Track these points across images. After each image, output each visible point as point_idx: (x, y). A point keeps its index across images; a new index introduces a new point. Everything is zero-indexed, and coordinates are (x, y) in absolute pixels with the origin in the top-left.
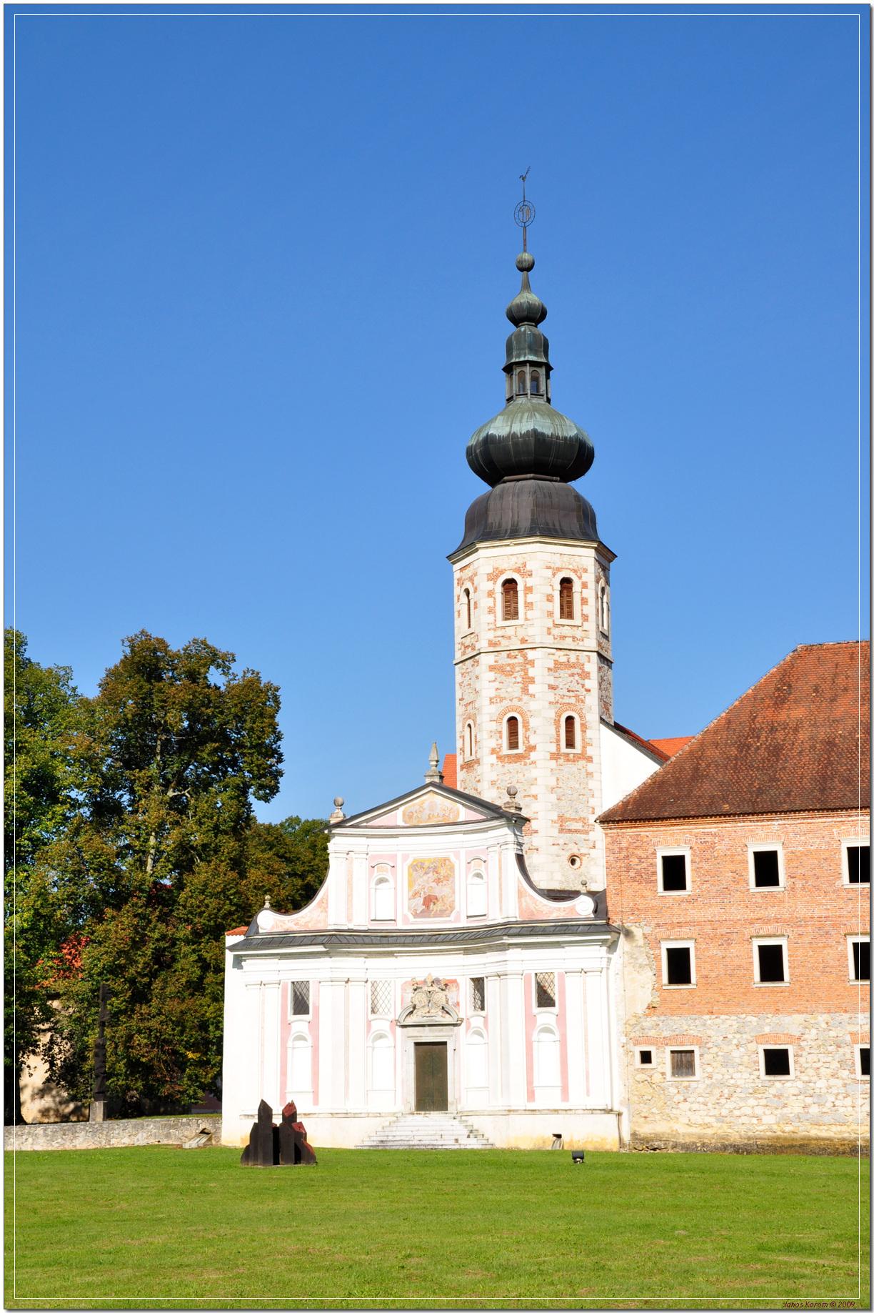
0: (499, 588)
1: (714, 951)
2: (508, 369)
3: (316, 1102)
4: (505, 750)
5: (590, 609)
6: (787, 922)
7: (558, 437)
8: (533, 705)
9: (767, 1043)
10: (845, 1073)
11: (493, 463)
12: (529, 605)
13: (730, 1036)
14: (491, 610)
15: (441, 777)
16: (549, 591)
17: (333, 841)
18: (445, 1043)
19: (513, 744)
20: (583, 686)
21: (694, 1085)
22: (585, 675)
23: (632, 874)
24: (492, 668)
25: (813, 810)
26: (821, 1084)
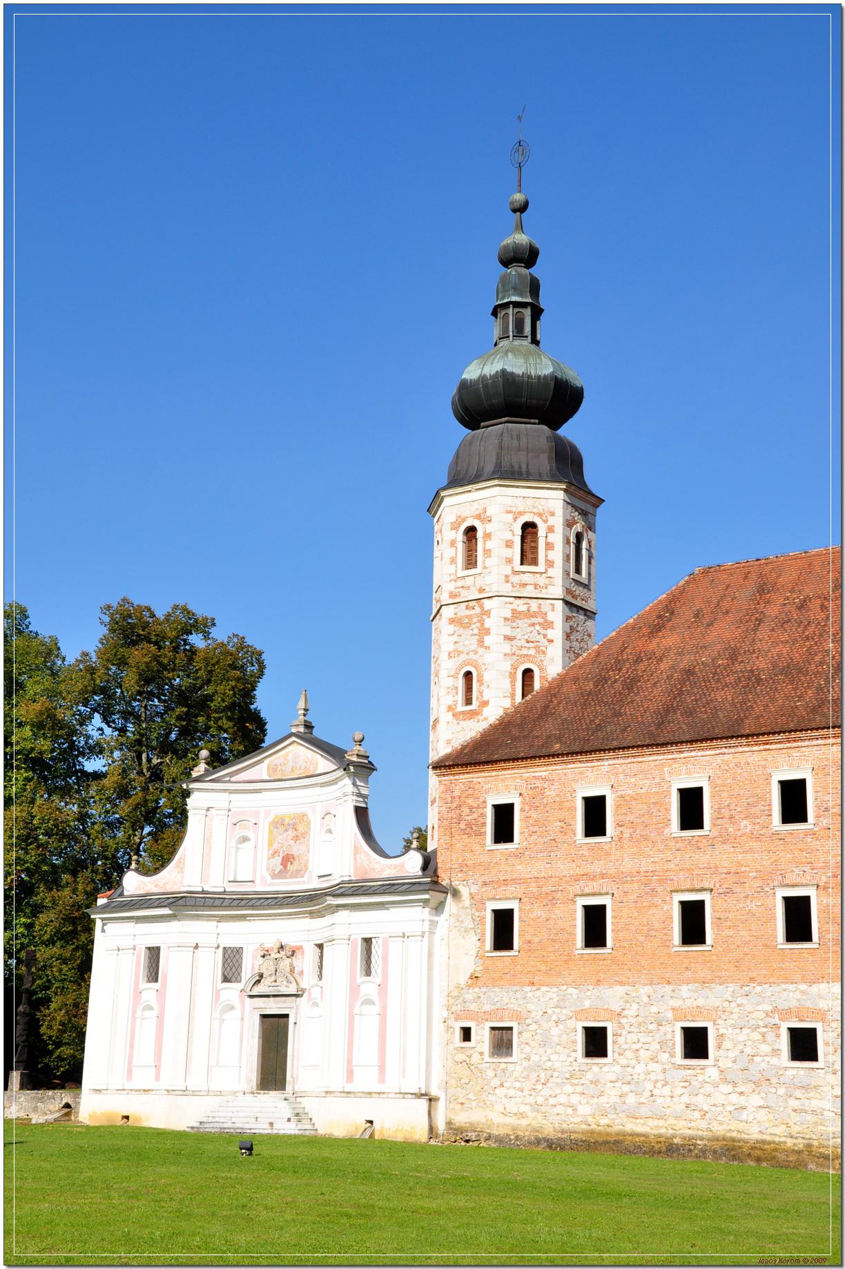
0: (460, 536)
1: (539, 912)
2: (495, 313)
3: (157, 1078)
4: (461, 707)
5: (557, 555)
6: (613, 878)
7: (529, 377)
9: (586, 1019)
10: (664, 1057)
11: (477, 408)
12: (487, 552)
13: (550, 1011)
16: (509, 536)
17: (192, 796)
19: (468, 701)
20: (545, 636)
21: (511, 1067)
22: (548, 625)
23: (463, 826)
24: (452, 621)
25: (643, 746)
26: (640, 1068)
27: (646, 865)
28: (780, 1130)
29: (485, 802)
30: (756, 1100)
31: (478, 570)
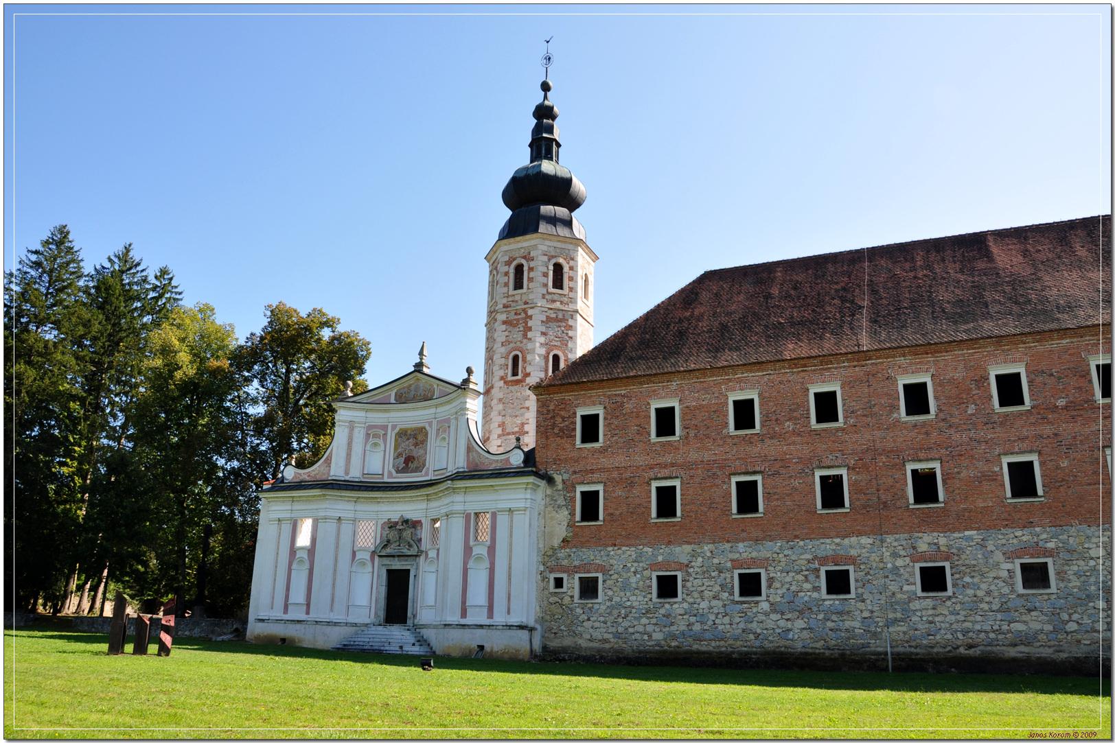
3: (308, 613)
4: (510, 378)
9: (660, 570)
14: (506, 285)
19: (515, 373)
21: (596, 606)
23: (556, 431)
24: (504, 323)
26: (704, 605)
27: (707, 456)
30: (800, 624)
31: (524, 290)
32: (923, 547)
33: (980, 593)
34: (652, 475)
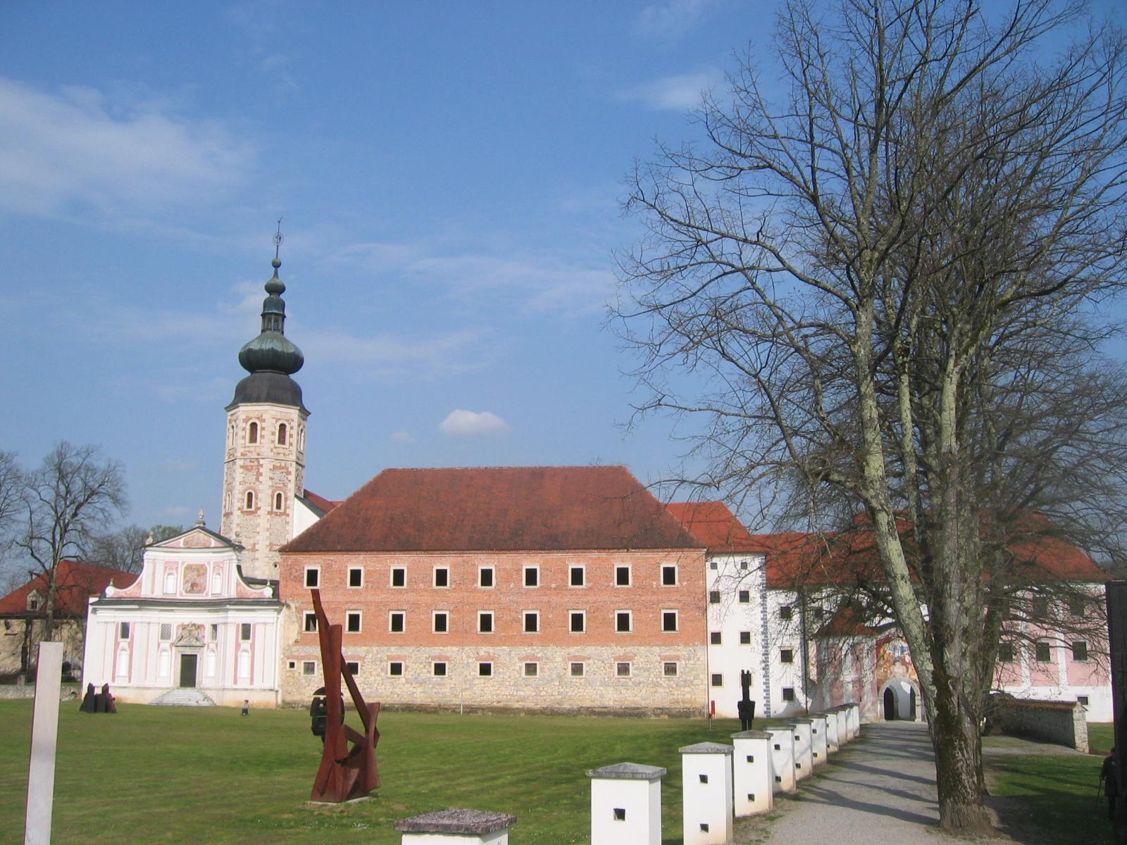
0: (248, 427)
3: (130, 681)
4: (245, 509)
5: (294, 440)
8: (261, 487)
10: (383, 674)
12: (262, 437)
14: (244, 437)
15: (204, 524)
16: (273, 430)
17: (146, 553)
18: (196, 656)
19: (249, 506)
22: (289, 473)
23: (292, 577)
24: (242, 467)
26: (372, 679)
27: (378, 599)
28: (428, 700)
29: (303, 568)
30: (420, 690)
32: (482, 653)
33: (506, 677)
34: (347, 607)
